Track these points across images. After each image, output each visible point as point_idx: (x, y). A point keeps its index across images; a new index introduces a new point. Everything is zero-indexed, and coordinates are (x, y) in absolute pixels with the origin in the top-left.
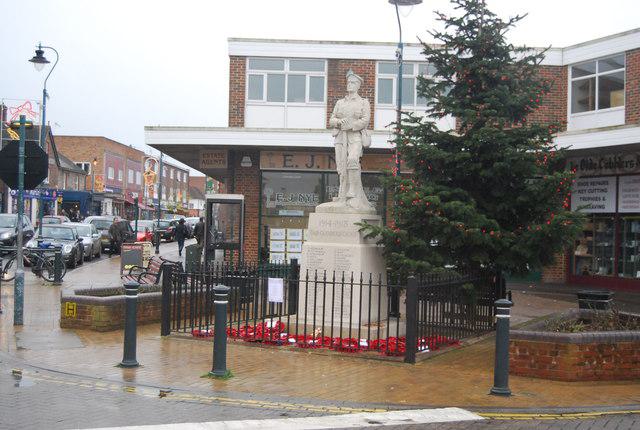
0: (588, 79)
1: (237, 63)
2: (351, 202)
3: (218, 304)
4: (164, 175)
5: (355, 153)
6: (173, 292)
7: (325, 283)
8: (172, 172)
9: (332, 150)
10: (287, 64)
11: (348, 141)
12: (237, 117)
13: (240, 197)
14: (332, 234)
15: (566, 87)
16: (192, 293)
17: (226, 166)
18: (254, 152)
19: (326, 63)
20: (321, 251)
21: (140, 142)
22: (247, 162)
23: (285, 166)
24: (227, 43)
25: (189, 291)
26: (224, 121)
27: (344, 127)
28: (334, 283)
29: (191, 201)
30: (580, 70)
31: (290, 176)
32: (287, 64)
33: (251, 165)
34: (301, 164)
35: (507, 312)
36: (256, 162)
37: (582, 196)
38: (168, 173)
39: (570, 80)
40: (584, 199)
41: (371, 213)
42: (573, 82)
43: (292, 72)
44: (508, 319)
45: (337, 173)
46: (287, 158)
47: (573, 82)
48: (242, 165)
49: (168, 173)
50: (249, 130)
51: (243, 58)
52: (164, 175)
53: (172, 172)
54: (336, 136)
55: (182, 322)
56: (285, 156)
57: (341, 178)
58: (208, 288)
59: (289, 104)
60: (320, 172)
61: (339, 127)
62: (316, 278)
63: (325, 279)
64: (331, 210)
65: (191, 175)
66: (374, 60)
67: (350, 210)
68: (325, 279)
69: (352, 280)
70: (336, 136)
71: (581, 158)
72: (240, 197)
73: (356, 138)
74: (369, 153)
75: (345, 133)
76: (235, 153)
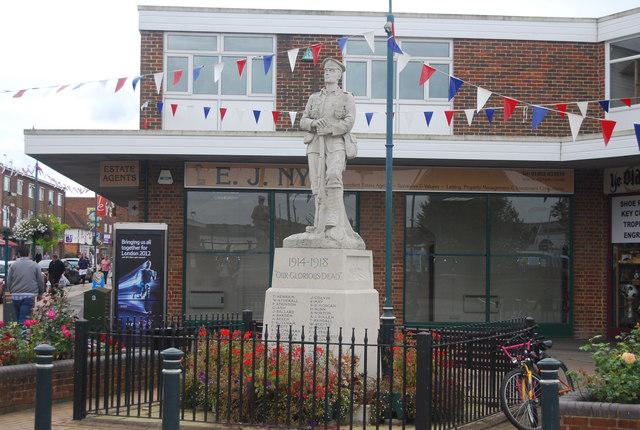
0: (632, 62)
1: (152, 43)
2: (332, 232)
3: (167, 375)
4: (30, 195)
5: (337, 166)
6: (89, 359)
7: (303, 343)
8: (51, 194)
9: (302, 161)
10: (220, 40)
11: (326, 149)
12: (152, 117)
13: (163, 227)
14: (305, 276)
15: (603, 72)
16: (128, 357)
17: (136, 183)
18: (177, 164)
19: (451, 43)
20: (290, 300)
21: (24, 164)
22: (166, 178)
23: (219, 183)
24: (137, 13)
25: (103, 358)
26: (134, 124)
27: (321, 131)
28: (366, 346)
29: (68, 232)
30: (629, 50)
31: (225, 196)
32: (220, 40)
33: (170, 182)
34: (243, 178)
35: (554, 376)
36: (179, 177)
37: (626, 219)
38: (36, 194)
39: (608, 62)
40: (629, 224)
41: (359, 247)
42: (611, 64)
43: (226, 53)
44: (557, 385)
45: (310, 192)
46: (222, 171)
47: (611, 64)
48: (160, 182)
49: (36, 194)
50: (170, 134)
51: (159, 34)
52: (30, 195)
53: (51, 194)
54: (309, 143)
55: (110, 398)
56: (219, 168)
57: (317, 200)
58: (128, 353)
59: (223, 97)
60: (283, 191)
61: (313, 130)
62: (290, 337)
63: (303, 337)
64: (306, 245)
65: (68, 194)
66: (163, 31)
67: (332, 243)
68: (303, 337)
69: (340, 339)
70: (309, 143)
71: (626, 168)
72: (163, 227)
73: (337, 145)
74: (355, 164)
75: (321, 140)
76: (149, 165)
